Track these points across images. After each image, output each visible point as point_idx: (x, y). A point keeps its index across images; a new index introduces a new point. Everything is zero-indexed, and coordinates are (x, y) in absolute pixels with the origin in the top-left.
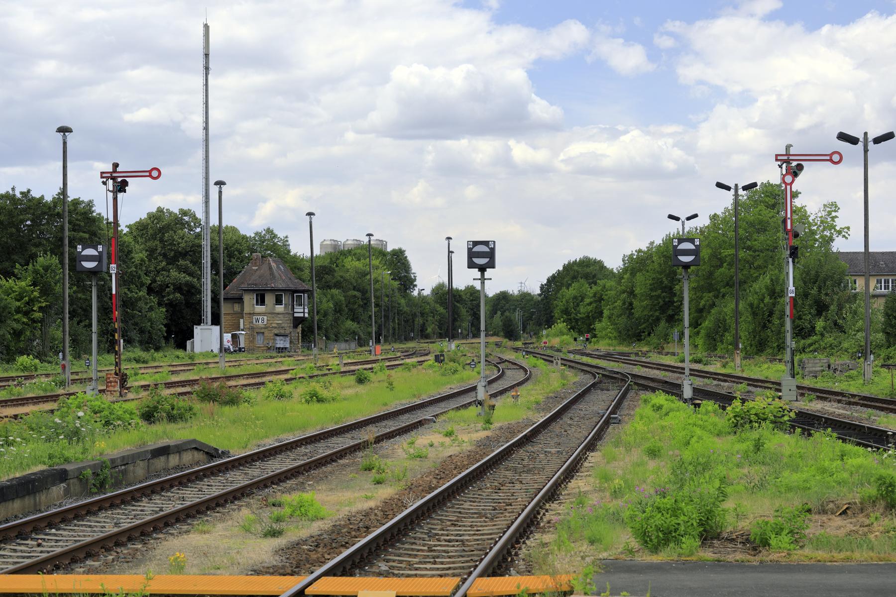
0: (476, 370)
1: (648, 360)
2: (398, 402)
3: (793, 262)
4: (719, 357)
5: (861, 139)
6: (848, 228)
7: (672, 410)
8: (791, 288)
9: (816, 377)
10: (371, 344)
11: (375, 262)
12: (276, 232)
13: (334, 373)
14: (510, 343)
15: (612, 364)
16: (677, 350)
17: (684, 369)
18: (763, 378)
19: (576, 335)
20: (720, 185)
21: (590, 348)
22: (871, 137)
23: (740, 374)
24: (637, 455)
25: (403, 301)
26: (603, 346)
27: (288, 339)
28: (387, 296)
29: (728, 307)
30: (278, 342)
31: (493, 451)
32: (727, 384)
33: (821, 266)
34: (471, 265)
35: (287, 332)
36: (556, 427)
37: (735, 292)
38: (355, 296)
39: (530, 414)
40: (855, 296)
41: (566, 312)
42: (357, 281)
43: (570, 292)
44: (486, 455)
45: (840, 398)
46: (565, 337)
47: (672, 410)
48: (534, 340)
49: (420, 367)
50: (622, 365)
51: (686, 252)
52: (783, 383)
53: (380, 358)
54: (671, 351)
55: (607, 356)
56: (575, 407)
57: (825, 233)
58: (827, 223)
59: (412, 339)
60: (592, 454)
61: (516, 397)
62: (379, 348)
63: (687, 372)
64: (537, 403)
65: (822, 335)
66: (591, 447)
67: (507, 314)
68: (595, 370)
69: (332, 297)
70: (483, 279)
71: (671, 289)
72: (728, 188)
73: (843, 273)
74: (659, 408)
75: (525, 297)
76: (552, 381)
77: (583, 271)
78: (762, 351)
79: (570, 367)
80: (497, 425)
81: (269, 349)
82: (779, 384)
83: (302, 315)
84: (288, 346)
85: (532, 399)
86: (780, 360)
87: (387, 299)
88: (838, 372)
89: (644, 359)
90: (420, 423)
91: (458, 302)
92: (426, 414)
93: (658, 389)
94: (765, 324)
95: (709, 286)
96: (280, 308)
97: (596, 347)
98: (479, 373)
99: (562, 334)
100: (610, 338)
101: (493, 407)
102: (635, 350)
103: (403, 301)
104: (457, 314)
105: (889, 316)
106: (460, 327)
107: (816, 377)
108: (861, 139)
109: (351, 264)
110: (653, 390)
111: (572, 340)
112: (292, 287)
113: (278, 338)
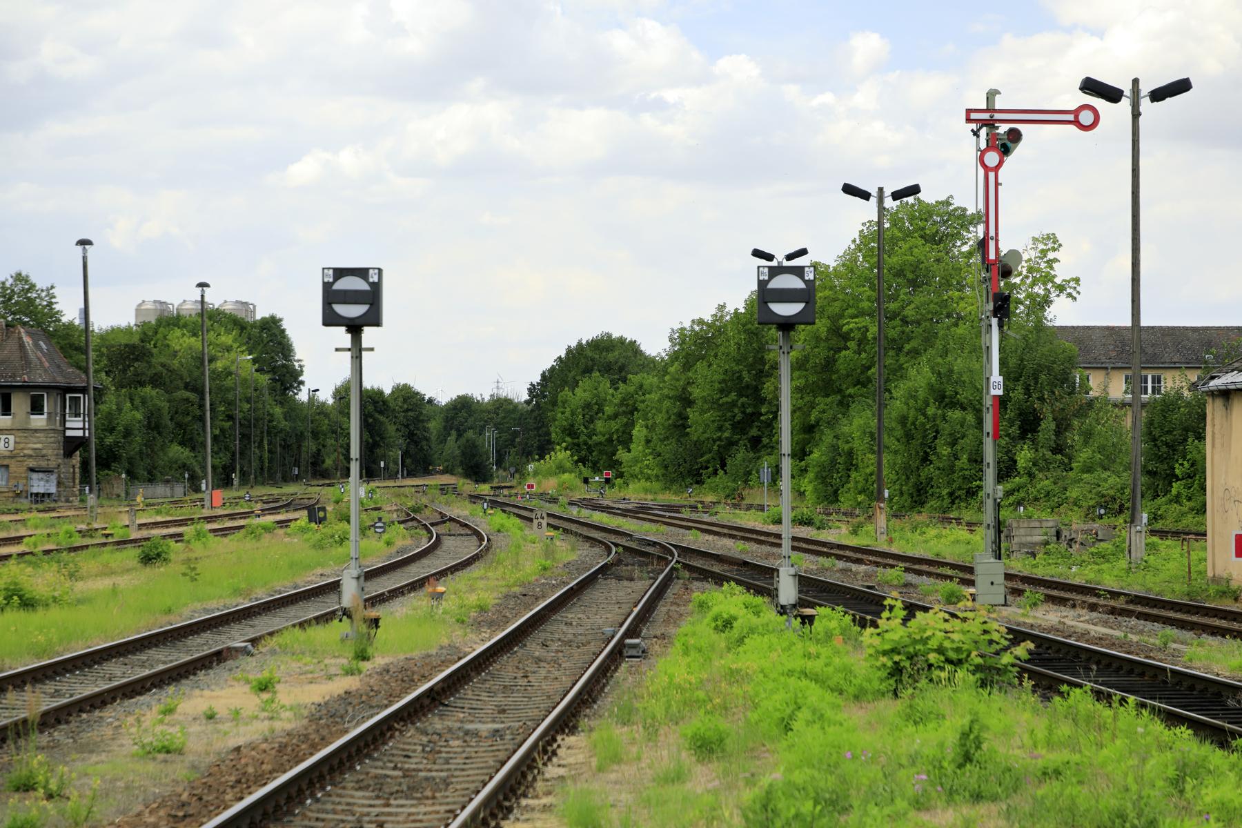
0: (385, 537)
1: (714, 519)
2: (198, 606)
3: (1001, 326)
4: (845, 514)
5: (1127, 92)
6: (1077, 280)
7: (752, 631)
8: (996, 377)
9: (1034, 555)
10: (203, 487)
11: (227, 339)
12: (34, 279)
13: (118, 543)
14: (467, 486)
15: (647, 526)
16: (766, 501)
17: (779, 536)
18: (929, 555)
19: (586, 472)
20: (849, 189)
21: (611, 497)
22: (1146, 88)
23: (884, 548)
24: (672, 749)
25: (278, 411)
26: (635, 493)
27: (54, 477)
28: (248, 400)
29: (857, 424)
30: (35, 483)
31: (346, 731)
32: (862, 568)
33: (1028, 348)
34: (330, 319)
35: (52, 464)
36: (506, 667)
37: (871, 400)
38: (187, 400)
39: (458, 636)
40: (1090, 404)
41: (571, 431)
42: (190, 372)
43: (582, 394)
44: (325, 741)
45: (1094, 600)
46: (566, 476)
47: (752, 631)
48: (514, 483)
49: (281, 532)
50: (663, 528)
51: (786, 296)
52: (979, 569)
53: (220, 512)
54: (757, 502)
55: (639, 512)
56: (557, 617)
57: (1036, 289)
58: (1038, 270)
59: (297, 479)
60: (571, 740)
61: (439, 596)
62: (220, 495)
63: (786, 544)
64: (482, 609)
65: (1031, 475)
66: (566, 723)
67: (470, 434)
68: (614, 539)
69: (144, 402)
70: (357, 350)
71: (757, 390)
72: (865, 196)
73: (1071, 362)
74: (727, 624)
75: (501, 406)
76: (527, 556)
77: (601, 360)
78: (923, 504)
79: (566, 531)
80: (379, 661)
81: (18, 495)
82: (970, 570)
83: (80, 433)
84: (53, 490)
85: (472, 599)
86: (958, 521)
87: (247, 406)
88: (1076, 546)
89: (706, 518)
90: (219, 657)
91: (381, 412)
92: (236, 637)
93: (728, 579)
94: (926, 454)
95: (828, 383)
96: (39, 421)
97: (622, 495)
98: (388, 543)
99: (561, 469)
100: (648, 478)
101: (375, 622)
102: (692, 501)
103: (278, 411)
104: (380, 435)
105: (1154, 440)
106: (384, 457)
107: (1034, 555)
108: (1127, 92)
109: (181, 342)
110: (719, 580)
111: (579, 482)
112: (61, 381)
113: (35, 476)
